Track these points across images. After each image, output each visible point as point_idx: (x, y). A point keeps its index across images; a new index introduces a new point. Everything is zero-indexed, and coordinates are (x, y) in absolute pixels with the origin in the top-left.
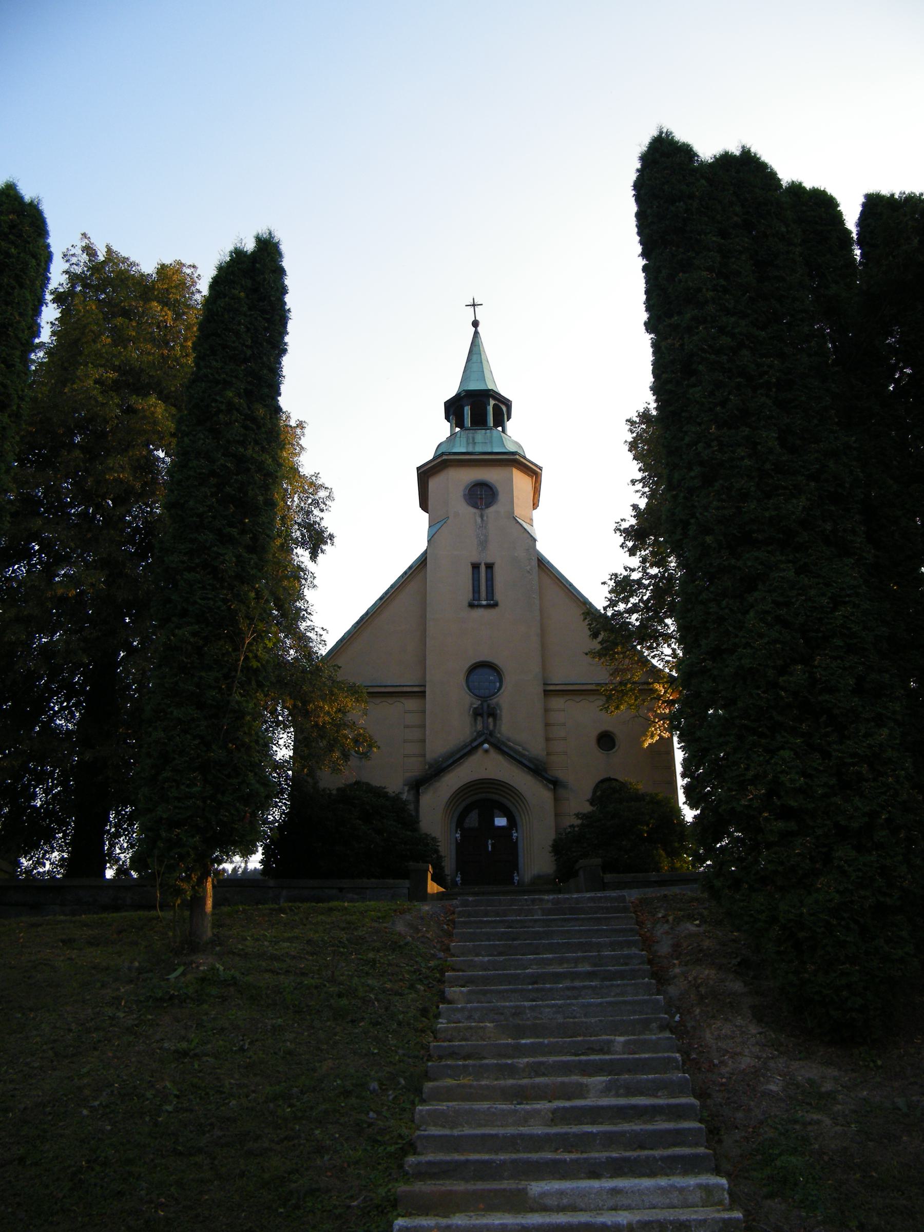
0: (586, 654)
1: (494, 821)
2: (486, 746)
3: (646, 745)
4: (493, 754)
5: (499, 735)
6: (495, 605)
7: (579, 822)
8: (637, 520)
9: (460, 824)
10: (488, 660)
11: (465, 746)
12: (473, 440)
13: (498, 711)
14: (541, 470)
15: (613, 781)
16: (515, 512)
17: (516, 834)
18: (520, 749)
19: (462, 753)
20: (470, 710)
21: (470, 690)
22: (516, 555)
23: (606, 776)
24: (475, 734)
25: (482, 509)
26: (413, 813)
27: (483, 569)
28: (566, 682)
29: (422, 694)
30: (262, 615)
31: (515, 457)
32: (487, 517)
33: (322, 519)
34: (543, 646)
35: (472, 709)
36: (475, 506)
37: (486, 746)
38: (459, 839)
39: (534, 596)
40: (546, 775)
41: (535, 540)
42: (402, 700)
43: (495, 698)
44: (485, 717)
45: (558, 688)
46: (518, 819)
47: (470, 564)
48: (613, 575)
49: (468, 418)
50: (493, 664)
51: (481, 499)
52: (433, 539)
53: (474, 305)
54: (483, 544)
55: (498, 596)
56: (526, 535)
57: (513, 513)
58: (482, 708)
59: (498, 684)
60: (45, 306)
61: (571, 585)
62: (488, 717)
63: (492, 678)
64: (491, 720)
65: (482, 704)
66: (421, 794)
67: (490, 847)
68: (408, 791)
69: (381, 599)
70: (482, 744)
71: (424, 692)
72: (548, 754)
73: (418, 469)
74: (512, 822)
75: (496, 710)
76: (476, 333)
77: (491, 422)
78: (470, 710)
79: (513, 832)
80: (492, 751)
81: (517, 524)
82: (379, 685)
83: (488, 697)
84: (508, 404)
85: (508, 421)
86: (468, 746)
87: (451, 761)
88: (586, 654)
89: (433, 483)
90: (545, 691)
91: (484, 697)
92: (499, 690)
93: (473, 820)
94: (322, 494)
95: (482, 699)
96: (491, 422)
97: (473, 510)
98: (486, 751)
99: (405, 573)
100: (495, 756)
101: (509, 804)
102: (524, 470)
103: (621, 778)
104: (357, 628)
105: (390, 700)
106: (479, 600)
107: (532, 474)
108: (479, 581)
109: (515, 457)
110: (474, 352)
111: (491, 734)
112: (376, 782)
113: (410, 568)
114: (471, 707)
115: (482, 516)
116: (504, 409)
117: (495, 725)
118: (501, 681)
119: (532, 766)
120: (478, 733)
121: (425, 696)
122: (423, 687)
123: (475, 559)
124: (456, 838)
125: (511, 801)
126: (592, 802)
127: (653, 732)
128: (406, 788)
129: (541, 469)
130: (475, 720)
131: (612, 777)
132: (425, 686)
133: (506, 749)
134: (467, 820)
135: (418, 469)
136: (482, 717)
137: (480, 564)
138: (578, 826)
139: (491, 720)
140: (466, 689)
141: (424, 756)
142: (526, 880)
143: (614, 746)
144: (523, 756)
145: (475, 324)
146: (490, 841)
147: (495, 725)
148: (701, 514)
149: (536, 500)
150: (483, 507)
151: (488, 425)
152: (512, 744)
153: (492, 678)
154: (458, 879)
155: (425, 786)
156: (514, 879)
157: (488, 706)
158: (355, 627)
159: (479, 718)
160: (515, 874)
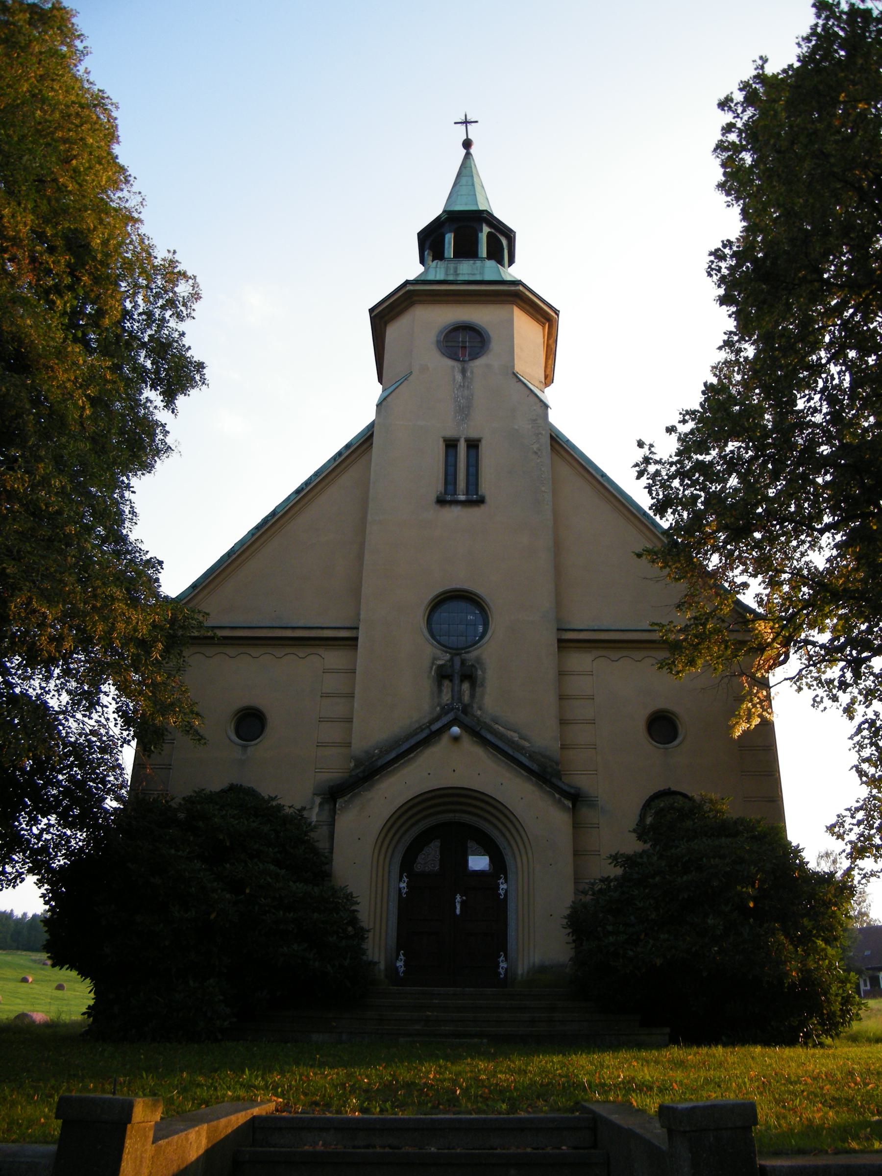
0: (639, 556)
1: (467, 861)
2: (456, 730)
3: (737, 733)
4: (468, 745)
5: (479, 713)
6: (481, 501)
7: (619, 871)
9: (407, 866)
11: (421, 729)
13: (480, 672)
14: (558, 315)
15: (679, 797)
16: (516, 366)
17: (504, 886)
18: (515, 737)
19: (413, 741)
21: (433, 637)
22: (516, 427)
23: (662, 787)
24: (438, 709)
25: (463, 361)
26: (323, 845)
27: (462, 447)
28: (596, 628)
29: (352, 642)
31: (517, 288)
32: (472, 373)
33: (183, 334)
34: (558, 570)
35: (434, 667)
36: (454, 357)
37: (456, 730)
39: (543, 489)
40: (560, 784)
41: (546, 406)
42: (321, 651)
43: (476, 649)
44: (457, 680)
47: (441, 440)
48: (687, 413)
49: (449, 247)
50: (476, 594)
51: (464, 348)
52: (384, 403)
53: (466, 122)
54: (464, 410)
55: (486, 486)
56: (532, 399)
57: (513, 366)
58: (452, 666)
59: (480, 629)
61: (604, 475)
62: (462, 681)
63: (470, 617)
64: (466, 686)
65: (451, 660)
66: (338, 812)
68: (321, 804)
69: (298, 492)
70: (449, 726)
71: (356, 639)
72: (563, 747)
74: (499, 865)
75: (476, 670)
76: (468, 155)
77: (483, 251)
81: (520, 383)
82: (284, 626)
83: (463, 649)
84: (510, 235)
85: (509, 266)
86: (424, 729)
87: (393, 755)
88: (639, 556)
89: (392, 332)
90: (560, 641)
91: (457, 649)
94: (183, 289)
95: (454, 652)
96: (483, 251)
97: (450, 363)
98: (456, 739)
99: (339, 454)
100: (470, 747)
101: (494, 834)
102: (531, 310)
103: (695, 793)
105: (302, 652)
106: (455, 493)
107: (543, 320)
108: (455, 466)
109: (517, 288)
111: (466, 710)
112: (265, 790)
113: (347, 446)
114: (433, 663)
115: (463, 372)
116: (504, 242)
117: (472, 696)
118: (486, 625)
119: (535, 767)
120: (443, 708)
121: (357, 645)
122: (355, 631)
123: (450, 433)
124: (400, 889)
125: (498, 829)
126: (641, 832)
127: (749, 710)
128: (318, 800)
129: (557, 312)
130: (440, 685)
131: (673, 789)
132: (357, 628)
133: (489, 737)
134: (420, 859)
136: (451, 681)
137: (460, 438)
138: (616, 879)
139: (466, 686)
141: (348, 745)
142: (520, 972)
143: (675, 738)
144: (520, 749)
145: (467, 144)
146: (458, 898)
147: (472, 696)
149: (549, 370)
150: (467, 358)
151: (479, 256)
152: (500, 728)
153: (470, 617)
154: (400, 964)
155: (346, 798)
156: (498, 967)
157: (463, 662)
158: (253, 535)
159: (446, 683)
160: (502, 958)
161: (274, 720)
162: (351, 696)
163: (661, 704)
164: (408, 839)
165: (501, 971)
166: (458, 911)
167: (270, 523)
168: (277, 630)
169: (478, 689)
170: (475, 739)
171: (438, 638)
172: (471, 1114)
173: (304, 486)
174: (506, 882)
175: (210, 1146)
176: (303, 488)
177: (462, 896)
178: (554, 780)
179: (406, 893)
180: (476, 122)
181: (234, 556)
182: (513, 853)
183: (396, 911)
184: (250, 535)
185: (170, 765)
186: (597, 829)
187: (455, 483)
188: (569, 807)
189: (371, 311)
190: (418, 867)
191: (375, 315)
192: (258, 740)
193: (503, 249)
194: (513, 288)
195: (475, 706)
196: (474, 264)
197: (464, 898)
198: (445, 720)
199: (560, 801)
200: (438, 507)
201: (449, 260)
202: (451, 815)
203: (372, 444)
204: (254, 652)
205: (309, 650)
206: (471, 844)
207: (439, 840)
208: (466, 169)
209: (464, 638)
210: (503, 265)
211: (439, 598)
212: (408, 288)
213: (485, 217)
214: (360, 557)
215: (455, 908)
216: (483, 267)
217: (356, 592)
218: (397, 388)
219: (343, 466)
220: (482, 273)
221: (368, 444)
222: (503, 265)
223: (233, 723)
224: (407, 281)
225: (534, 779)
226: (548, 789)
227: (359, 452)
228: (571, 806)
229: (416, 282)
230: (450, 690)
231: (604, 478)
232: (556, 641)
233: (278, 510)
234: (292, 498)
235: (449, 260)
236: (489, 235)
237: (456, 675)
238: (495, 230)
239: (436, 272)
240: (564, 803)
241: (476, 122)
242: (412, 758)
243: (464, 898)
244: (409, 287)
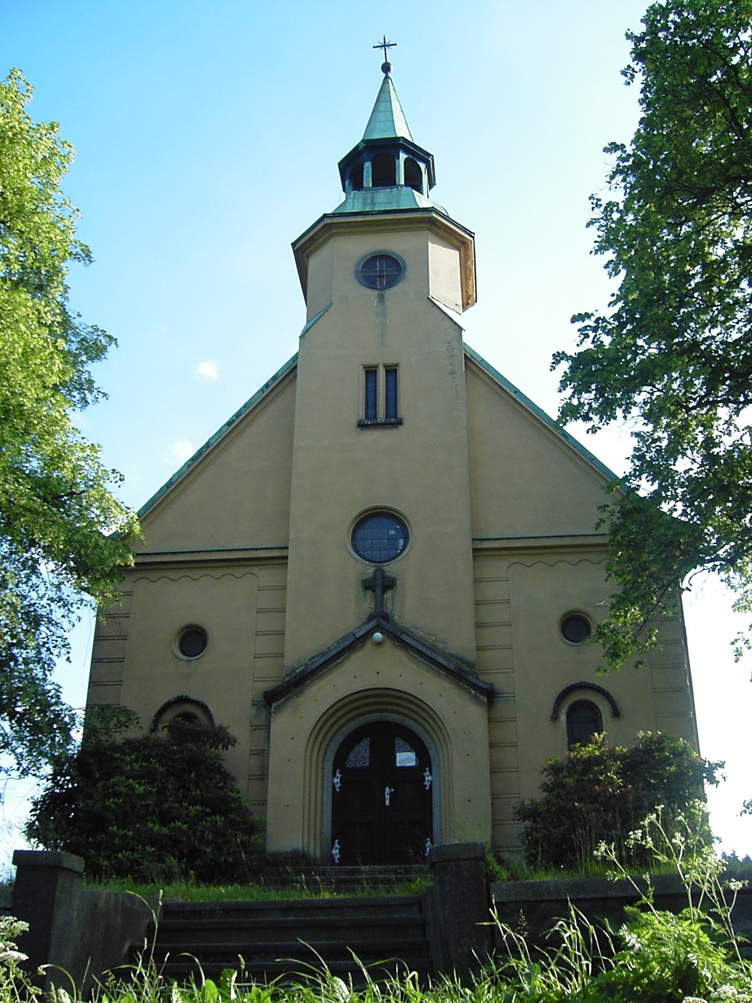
2: (378, 635)
6: (399, 423)
8: (631, 408)
9: (340, 762)
10: (387, 505)
12: (372, 201)
14: (473, 237)
21: (357, 552)
40: (475, 681)
42: (255, 570)
45: (497, 544)
46: (432, 754)
53: (385, 46)
55: (404, 411)
60: (716, 841)
61: (517, 391)
67: (387, 797)
70: (370, 633)
71: (286, 557)
72: (479, 649)
73: (293, 245)
74: (424, 760)
76: (387, 78)
79: (425, 774)
80: (388, 643)
81: (435, 307)
84: (426, 157)
89: (313, 264)
90: (474, 550)
92: (402, 551)
93: (361, 755)
98: (379, 644)
99: (267, 385)
104: (192, 468)
105: (238, 572)
110: (381, 100)
113: (274, 378)
115: (381, 298)
116: (422, 166)
118: (406, 538)
119: (452, 666)
121: (287, 564)
123: (371, 361)
124: (334, 784)
125: (419, 723)
129: (471, 234)
132: (287, 548)
133: (409, 640)
134: (352, 756)
135: (293, 245)
136: (374, 591)
137: (377, 366)
145: (386, 68)
146: (387, 789)
151: (397, 183)
161: (215, 635)
162: (283, 610)
163: (574, 604)
164: (340, 738)
167: (204, 455)
168: (203, 554)
170: (396, 643)
171: (362, 553)
172: (284, 883)
173: (235, 418)
174: (431, 771)
175: (407, 746)
176: (233, 420)
177: (390, 788)
178: (470, 678)
179: (340, 788)
180: (396, 45)
181: (173, 487)
183: (330, 803)
184: (187, 466)
185: (122, 681)
187: (375, 408)
188: (484, 702)
189: (293, 245)
191: (297, 249)
192: (201, 655)
193: (421, 173)
194: (426, 215)
196: (391, 192)
197: (393, 790)
198: (368, 627)
200: (359, 430)
201: (368, 189)
202: (378, 715)
203: (296, 376)
204: (195, 574)
205: (181, 573)
206: (399, 742)
207: (369, 739)
208: (383, 97)
210: (420, 191)
211: (363, 516)
212: (325, 222)
213: (397, 144)
214: (289, 482)
216: (399, 195)
217: (285, 514)
218: (317, 321)
219: (270, 398)
220: (398, 202)
221: (291, 377)
222: (420, 191)
223: (177, 642)
224: (325, 214)
227: (285, 383)
228: (486, 701)
229: (334, 215)
231: (517, 394)
232: (471, 551)
233: (211, 442)
234: (224, 430)
235: (368, 189)
236: (406, 160)
238: (411, 154)
239: (354, 203)
241: (396, 45)
243: (393, 790)
244: (328, 221)
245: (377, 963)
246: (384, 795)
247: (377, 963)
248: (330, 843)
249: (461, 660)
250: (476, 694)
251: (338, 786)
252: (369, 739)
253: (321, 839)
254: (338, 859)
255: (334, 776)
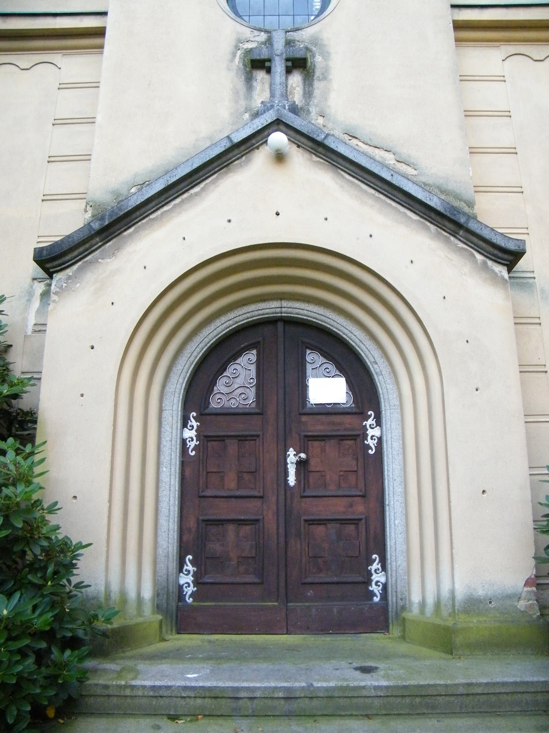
1: (303, 389)
17: (376, 432)
20: (234, 55)
30: (520, 677)
35: (239, 53)
38: (192, 445)
62: (289, 71)
75: (314, 56)
78: (234, 55)
114: (237, 48)
117: (308, 94)
124: (184, 442)
130: (249, 79)
134: (221, 386)
136: (269, 71)
139: (296, 79)
140: (233, 15)
146: (291, 452)
147: (308, 94)
148: (492, 605)
155: (69, 272)
156: (368, 582)
159: (260, 75)
160: (376, 566)
165: (376, 589)
166: (292, 480)
169: (316, 84)
175: (332, 367)
179: (196, 448)
182: (393, 371)
186: (538, 327)
188: (503, 278)
190: (215, 403)
195: (313, 110)
197: (303, 455)
199: (484, 265)
202: (275, 304)
207: (254, 352)
209: (290, 19)
215: (286, 474)
225: (432, 227)
226: (461, 245)
230: (267, 86)
237: (277, 58)
240: (493, 271)
242: (197, 194)
243: (303, 455)
245: (206, 604)
246: (286, 464)
247: (206, 604)
248: (173, 565)
249: (457, 197)
250: (485, 263)
251: (192, 445)
252: (254, 352)
253: (155, 562)
254: (191, 596)
255: (185, 425)
